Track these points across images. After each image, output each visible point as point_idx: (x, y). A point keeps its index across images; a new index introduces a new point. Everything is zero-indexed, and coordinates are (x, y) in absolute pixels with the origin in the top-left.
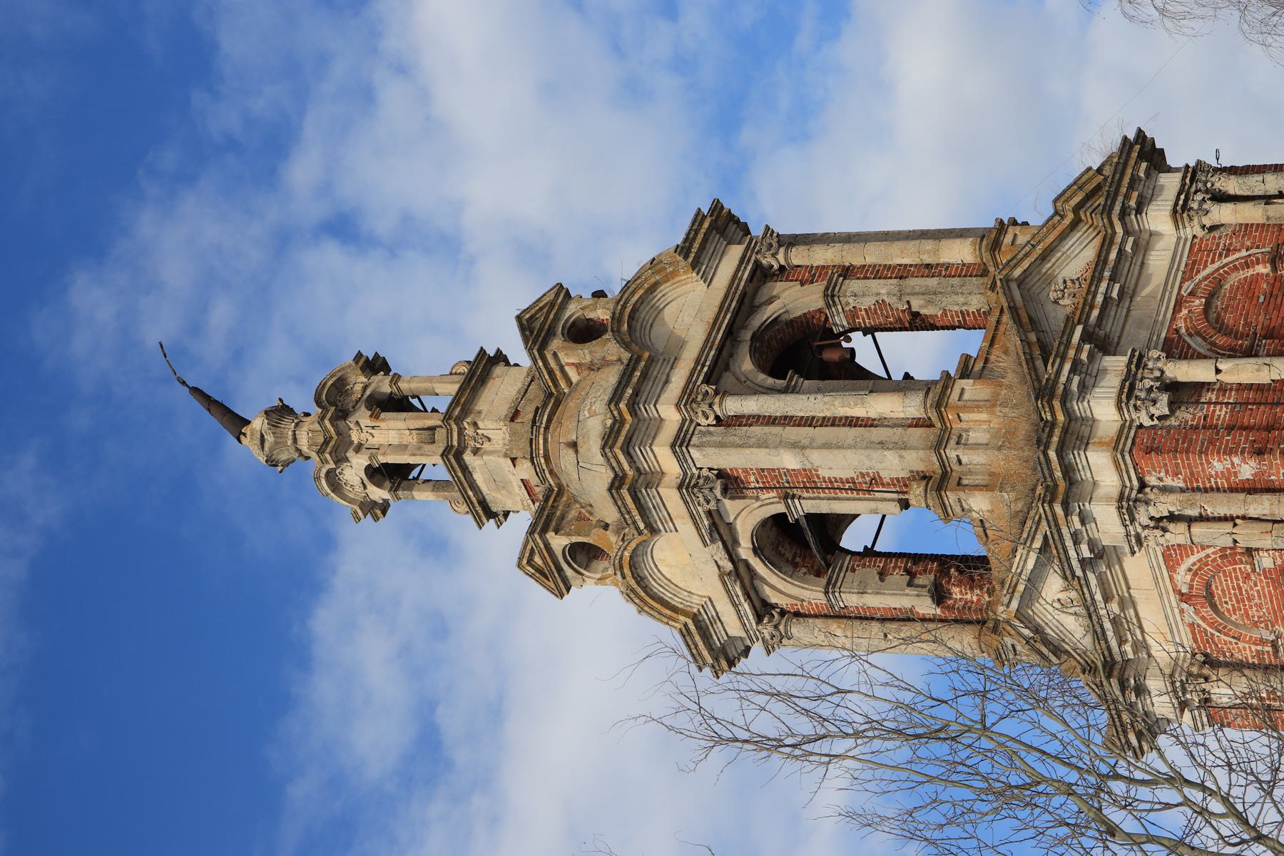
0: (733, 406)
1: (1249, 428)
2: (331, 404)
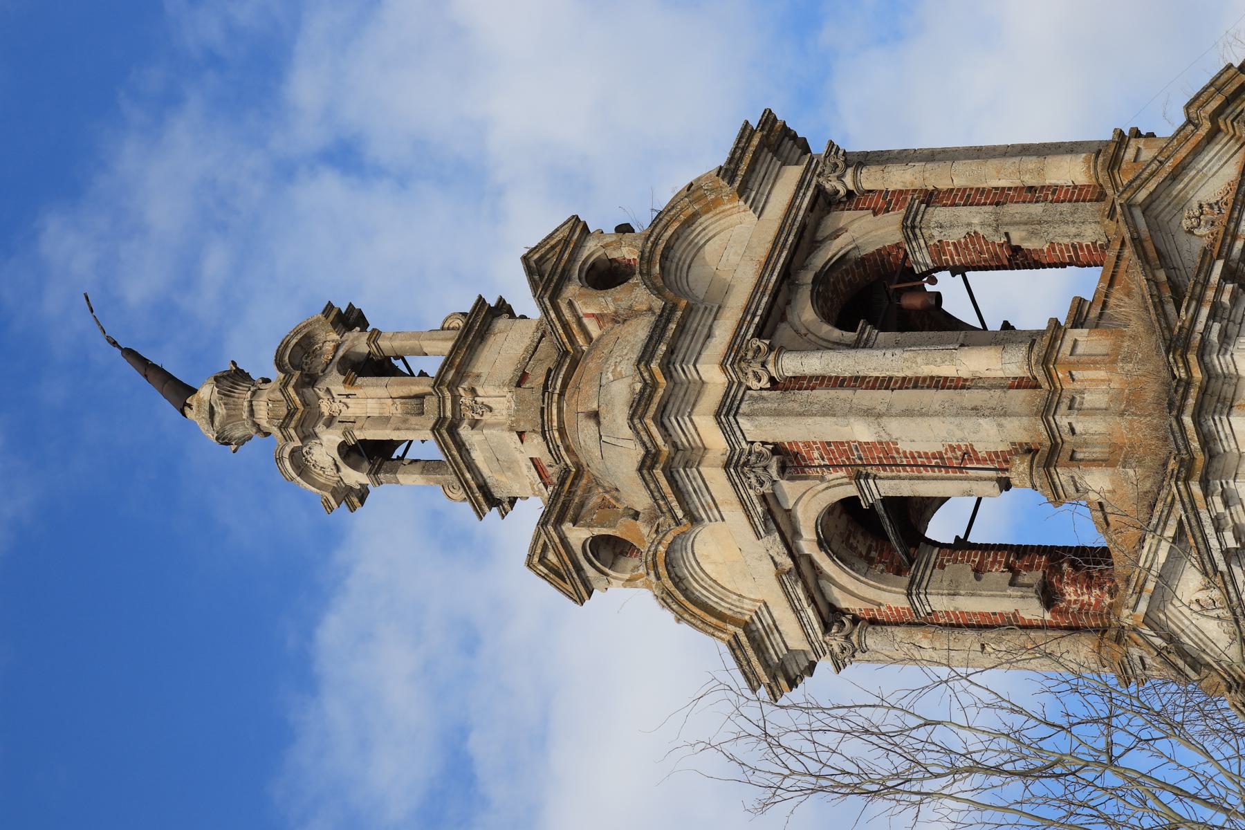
0: (791, 364)
2: (295, 367)
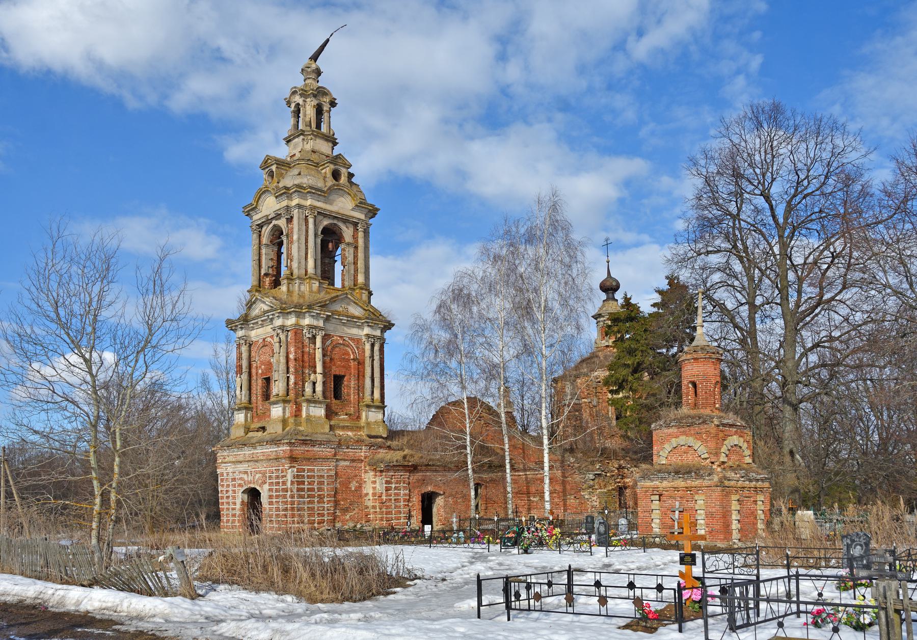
0: (311, 221)
1: (303, 356)
2: (318, 92)
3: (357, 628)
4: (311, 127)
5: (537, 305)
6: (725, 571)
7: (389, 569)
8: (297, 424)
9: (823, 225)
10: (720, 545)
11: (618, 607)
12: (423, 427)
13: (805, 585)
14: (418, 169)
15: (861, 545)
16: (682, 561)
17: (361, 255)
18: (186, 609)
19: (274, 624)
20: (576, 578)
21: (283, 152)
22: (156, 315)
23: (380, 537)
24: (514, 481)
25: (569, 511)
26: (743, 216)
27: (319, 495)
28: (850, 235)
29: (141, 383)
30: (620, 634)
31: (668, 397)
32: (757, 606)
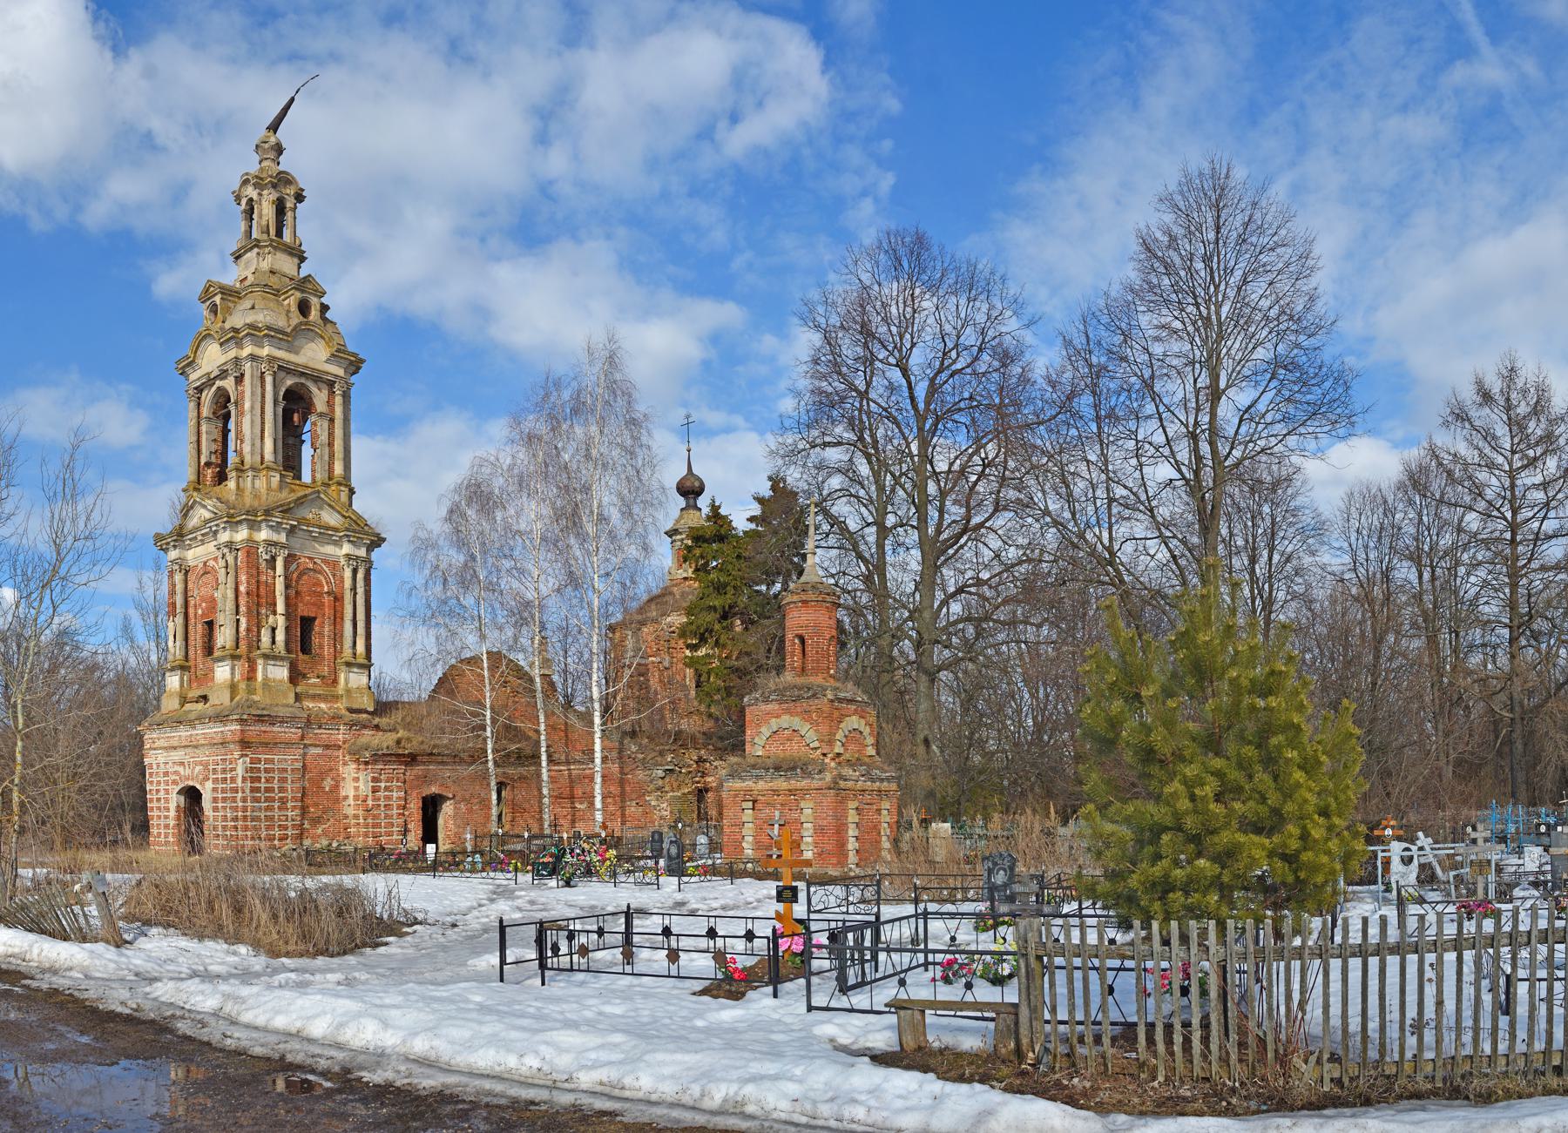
0: (269, 379)
1: (258, 587)
3: (338, 996)
4: (268, 233)
5: (587, 512)
6: (837, 910)
7: (378, 909)
8: (251, 691)
9: (973, 419)
10: (833, 872)
11: (695, 963)
12: (425, 696)
13: (935, 926)
14: (422, 305)
15: (1005, 870)
16: (780, 897)
17: (338, 432)
18: (110, 960)
19: (224, 987)
20: (639, 924)
21: (231, 276)
22: (66, 531)
23: (364, 860)
24: (552, 779)
25: (628, 824)
26: (872, 395)
27: (280, 798)
28: (1006, 436)
29: (47, 632)
30: (696, 1002)
31: (768, 658)
32: (875, 958)
